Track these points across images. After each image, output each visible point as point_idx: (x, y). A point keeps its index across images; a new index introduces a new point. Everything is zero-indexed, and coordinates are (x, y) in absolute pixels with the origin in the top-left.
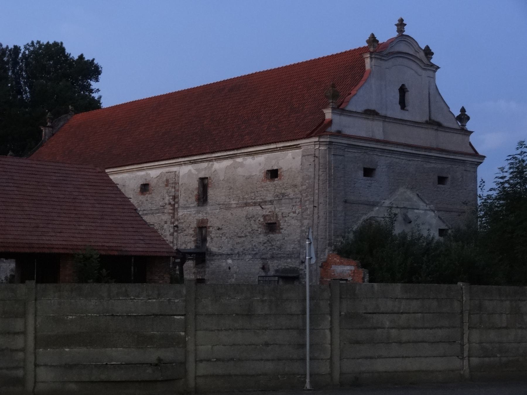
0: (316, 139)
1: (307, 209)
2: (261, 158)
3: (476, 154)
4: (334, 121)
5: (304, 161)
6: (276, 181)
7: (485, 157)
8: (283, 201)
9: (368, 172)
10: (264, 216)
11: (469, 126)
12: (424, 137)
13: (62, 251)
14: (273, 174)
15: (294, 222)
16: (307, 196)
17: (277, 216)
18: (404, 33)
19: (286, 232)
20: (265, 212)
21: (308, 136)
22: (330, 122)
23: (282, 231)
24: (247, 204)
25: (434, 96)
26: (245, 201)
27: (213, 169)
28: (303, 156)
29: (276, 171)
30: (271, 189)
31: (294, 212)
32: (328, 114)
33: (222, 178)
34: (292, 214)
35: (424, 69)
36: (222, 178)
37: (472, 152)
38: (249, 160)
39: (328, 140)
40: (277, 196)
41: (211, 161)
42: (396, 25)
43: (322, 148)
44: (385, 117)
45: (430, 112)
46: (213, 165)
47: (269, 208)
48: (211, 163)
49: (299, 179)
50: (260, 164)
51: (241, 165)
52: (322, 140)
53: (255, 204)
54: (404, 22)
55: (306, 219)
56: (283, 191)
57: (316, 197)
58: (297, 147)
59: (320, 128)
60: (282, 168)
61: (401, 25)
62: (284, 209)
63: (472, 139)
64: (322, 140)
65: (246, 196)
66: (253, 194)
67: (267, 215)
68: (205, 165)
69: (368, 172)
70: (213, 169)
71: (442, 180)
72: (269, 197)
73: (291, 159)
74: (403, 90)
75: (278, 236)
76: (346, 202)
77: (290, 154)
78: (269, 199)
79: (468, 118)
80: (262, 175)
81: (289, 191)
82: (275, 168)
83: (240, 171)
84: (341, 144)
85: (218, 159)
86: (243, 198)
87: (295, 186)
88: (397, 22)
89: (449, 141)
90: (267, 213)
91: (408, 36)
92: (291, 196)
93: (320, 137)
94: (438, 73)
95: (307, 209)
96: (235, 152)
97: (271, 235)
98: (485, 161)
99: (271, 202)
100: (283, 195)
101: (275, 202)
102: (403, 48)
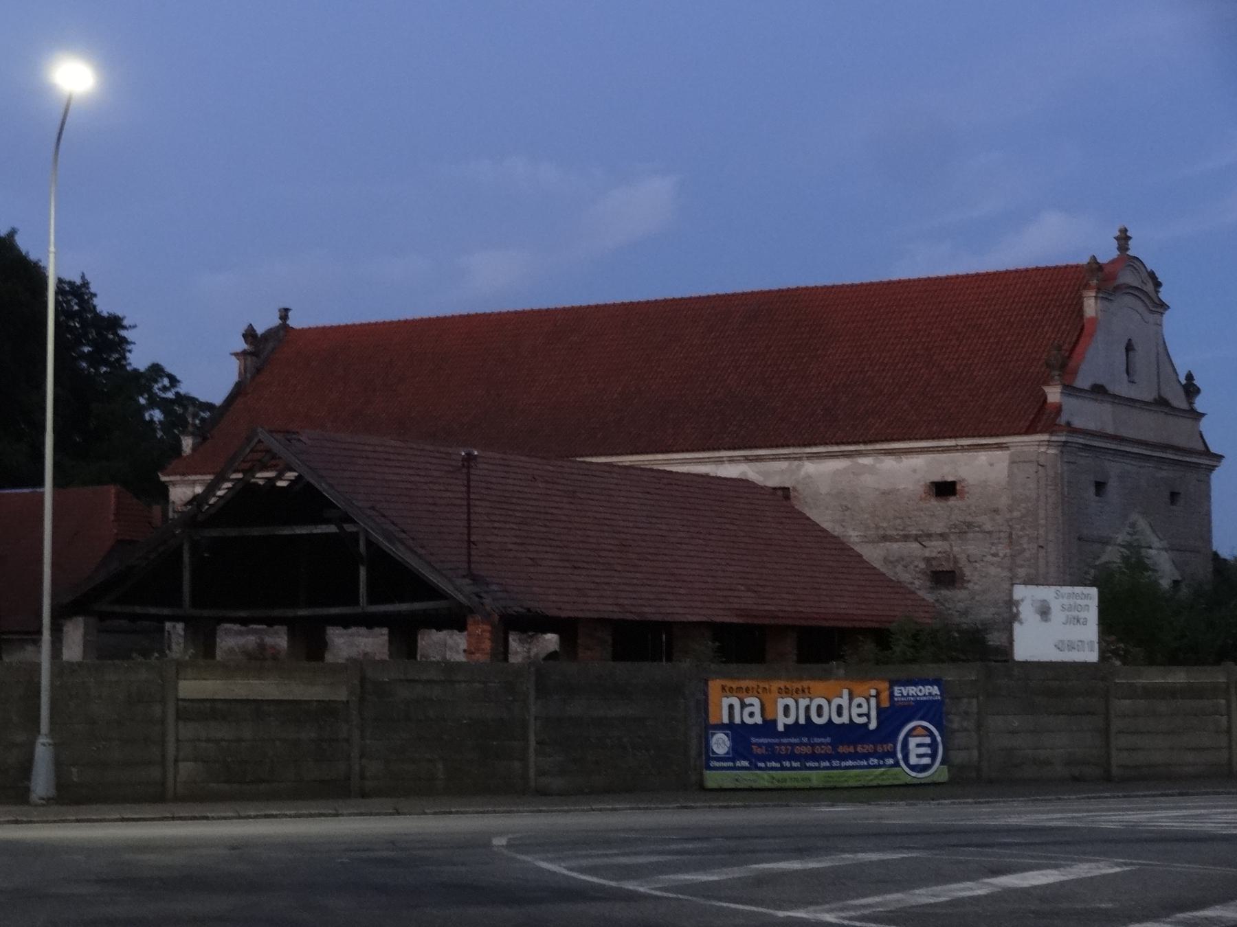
0: (1045, 437)
1: (1024, 550)
2: (918, 461)
3: (1207, 453)
4: (1064, 407)
5: (1016, 470)
6: (952, 501)
7: (1221, 457)
8: (970, 535)
9: (1100, 487)
10: (928, 560)
11: (1200, 404)
12: (1146, 426)
13: (766, 621)
14: (945, 489)
15: (993, 571)
16: (1023, 529)
17: (956, 561)
18: (1129, 253)
19: (976, 587)
20: (927, 553)
21: (1029, 431)
22: (1058, 409)
23: (970, 585)
24: (885, 538)
25: (1163, 356)
26: (881, 532)
27: (802, 473)
28: (1013, 462)
29: (953, 484)
30: (942, 513)
31: (994, 555)
32: (1054, 394)
33: (824, 490)
34: (989, 558)
35: (1151, 312)
36: (824, 490)
37: (1201, 447)
38: (889, 463)
39: (1063, 439)
40: (955, 526)
41: (800, 459)
42: (1117, 238)
43: (1052, 451)
44: (1115, 396)
45: (1159, 383)
46: (799, 468)
47: (936, 548)
48: (796, 463)
49: (1004, 501)
50: (915, 471)
51: (871, 470)
52: (1054, 438)
53: (906, 538)
54: (1129, 234)
55: (1022, 566)
56: (969, 519)
57: (1042, 531)
58: (1000, 447)
59: (1040, 418)
60: (964, 480)
61: (1123, 239)
62: (973, 547)
63: (1204, 425)
64: (1054, 438)
65: (885, 525)
66: (898, 521)
67: (934, 558)
68: (784, 465)
69: (1100, 487)
70: (802, 473)
71: (1174, 496)
72: (938, 527)
73: (984, 466)
74: (1129, 348)
75: (961, 594)
76: (1079, 539)
77: (983, 457)
78: (939, 531)
79: (1198, 391)
80: (920, 490)
81: (981, 519)
82: (950, 479)
83: (868, 480)
84: (1083, 446)
85: (818, 456)
86: (877, 527)
87: (996, 511)
88: (1118, 234)
89: (1176, 431)
90: (934, 555)
91: (1137, 258)
92: (988, 527)
93: (1051, 434)
94: (1167, 317)
95: (1024, 550)
96: (862, 447)
97: (944, 592)
98: (1223, 461)
99: (943, 536)
100: (969, 525)
101: (952, 537)
102: (1127, 278)
